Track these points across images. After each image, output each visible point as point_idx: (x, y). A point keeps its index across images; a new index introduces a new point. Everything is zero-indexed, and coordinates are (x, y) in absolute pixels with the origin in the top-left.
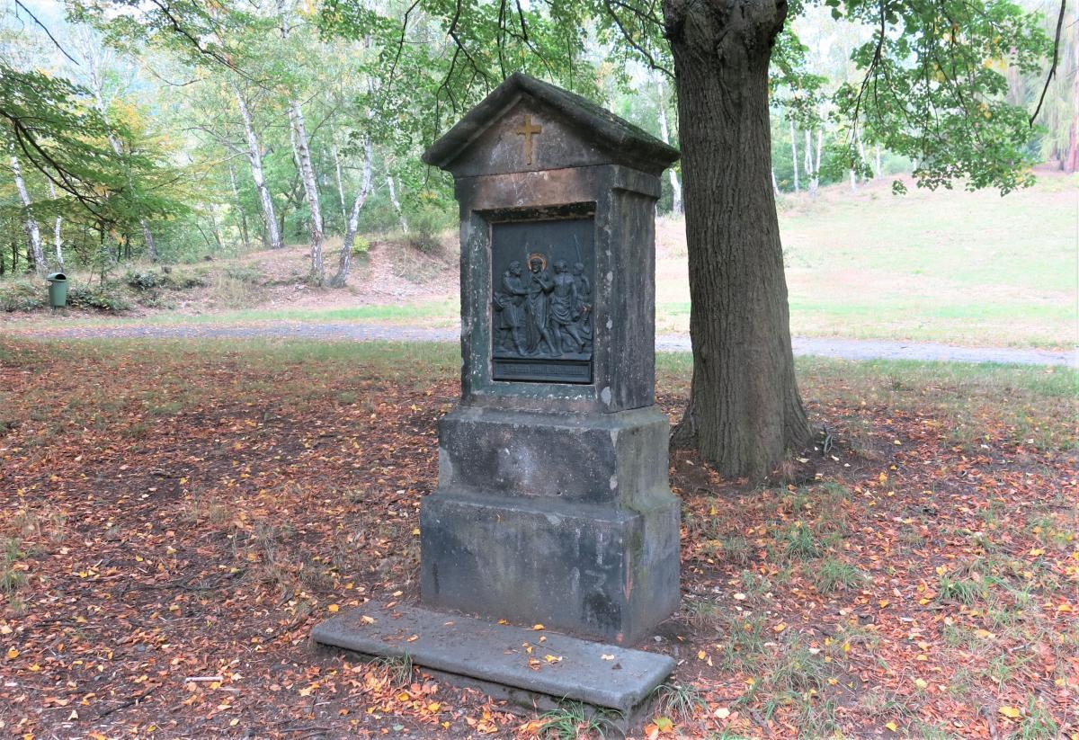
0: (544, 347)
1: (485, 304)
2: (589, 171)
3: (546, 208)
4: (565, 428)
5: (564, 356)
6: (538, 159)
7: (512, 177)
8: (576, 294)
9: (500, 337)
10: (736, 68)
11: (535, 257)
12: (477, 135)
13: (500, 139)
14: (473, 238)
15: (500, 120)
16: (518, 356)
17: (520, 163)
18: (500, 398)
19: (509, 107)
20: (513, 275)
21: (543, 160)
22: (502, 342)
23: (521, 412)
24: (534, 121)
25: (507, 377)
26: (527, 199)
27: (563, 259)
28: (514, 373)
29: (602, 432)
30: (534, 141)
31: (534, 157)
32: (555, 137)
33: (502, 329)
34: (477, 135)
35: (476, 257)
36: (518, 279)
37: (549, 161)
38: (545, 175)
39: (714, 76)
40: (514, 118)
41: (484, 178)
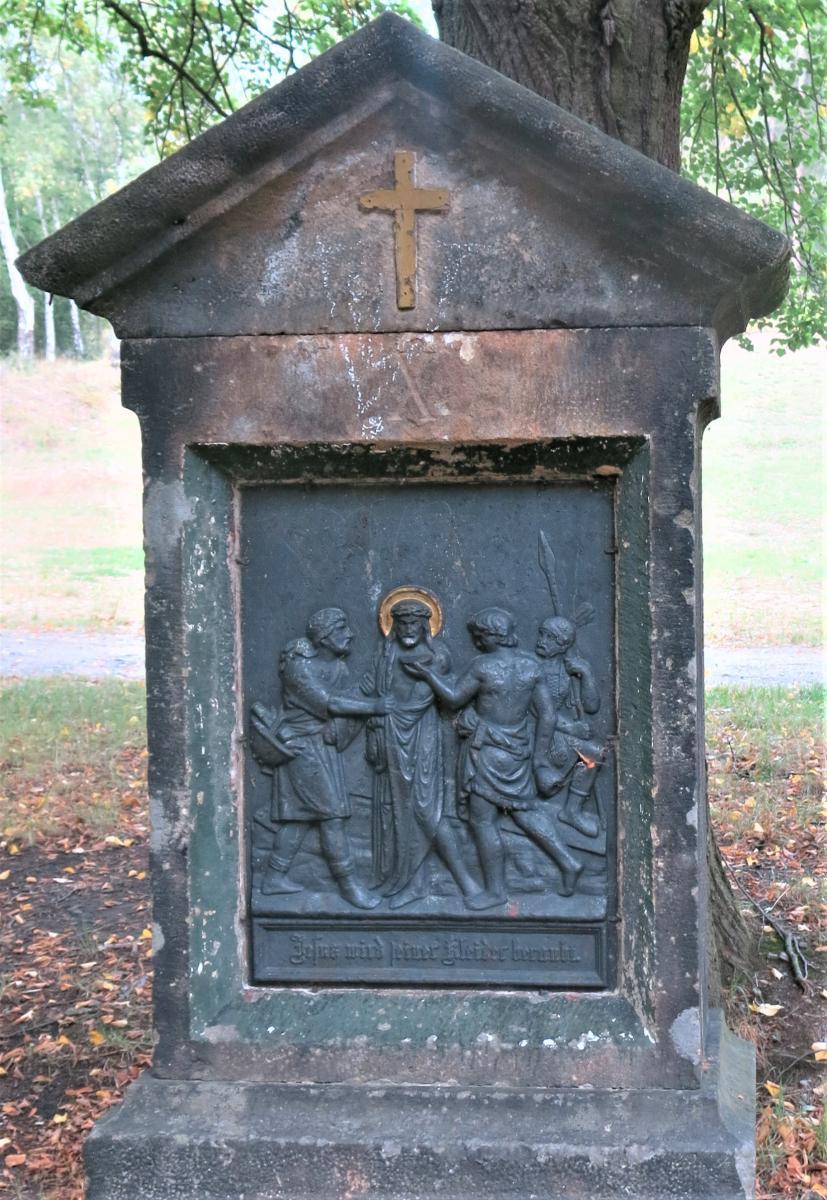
0: (436, 877)
1: (226, 745)
2: (621, 340)
3: (460, 448)
4: (573, 1150)
5: (513, 908)
6: (437, 294)
7: (343, 347)
8: (548, 716)
9: (275, 848)
10: (643, 70)
11: (403, 596)
12: (220, 206)
13: (297, 220)
14: (192, 536)
15: (309, 162)
16: (347, 910)
17: (373, 303)
18: (304, 1051)
19: (344, 124)
20: (324, 649)
21: (456, 298)
22: (283, 862)
23: (393, 1098)
24: (424, 173)
25: (304, 973)
26: (395, 418)
27: (501, 604)
28: (330, 959)
29: (707, 1161)
30: (424, 239)
31: (423, 288)
32: (500, 230)
33: (283, 822)
34: (220, 206)
35: (201, 594)
36: (340, 666)
37: (478, 303)
38: (468, 348)
39: (584, 83)
40: (352, 159)
41: (234, 344)
